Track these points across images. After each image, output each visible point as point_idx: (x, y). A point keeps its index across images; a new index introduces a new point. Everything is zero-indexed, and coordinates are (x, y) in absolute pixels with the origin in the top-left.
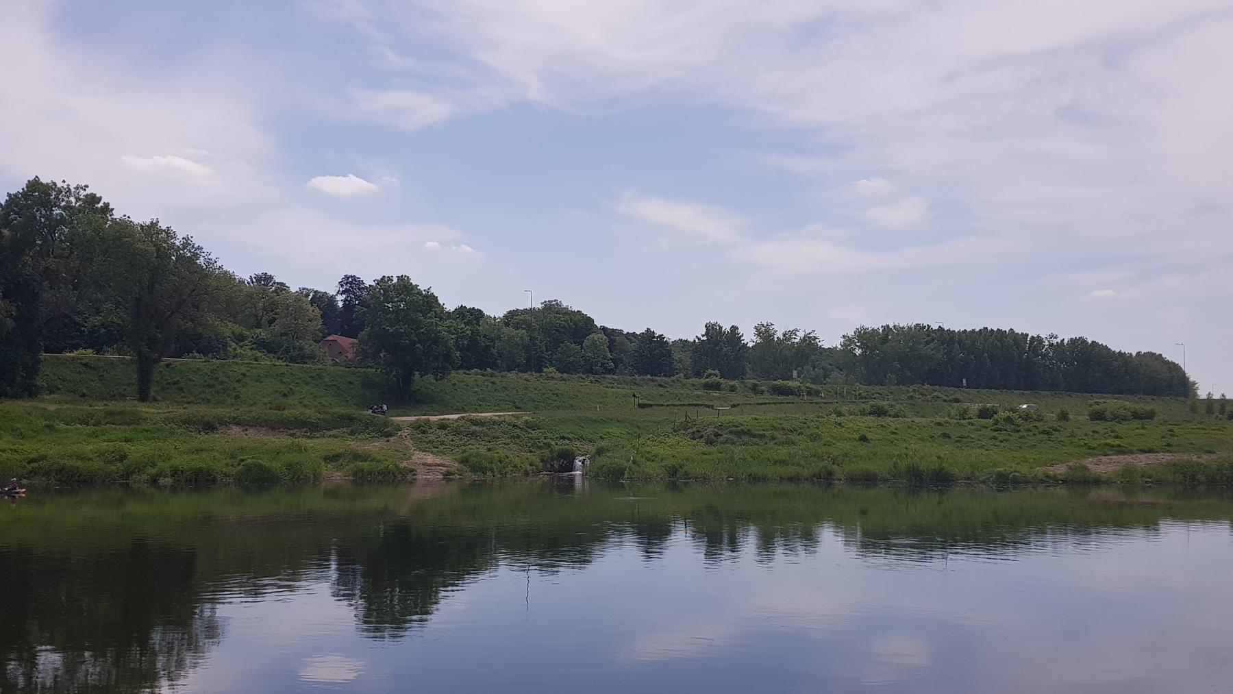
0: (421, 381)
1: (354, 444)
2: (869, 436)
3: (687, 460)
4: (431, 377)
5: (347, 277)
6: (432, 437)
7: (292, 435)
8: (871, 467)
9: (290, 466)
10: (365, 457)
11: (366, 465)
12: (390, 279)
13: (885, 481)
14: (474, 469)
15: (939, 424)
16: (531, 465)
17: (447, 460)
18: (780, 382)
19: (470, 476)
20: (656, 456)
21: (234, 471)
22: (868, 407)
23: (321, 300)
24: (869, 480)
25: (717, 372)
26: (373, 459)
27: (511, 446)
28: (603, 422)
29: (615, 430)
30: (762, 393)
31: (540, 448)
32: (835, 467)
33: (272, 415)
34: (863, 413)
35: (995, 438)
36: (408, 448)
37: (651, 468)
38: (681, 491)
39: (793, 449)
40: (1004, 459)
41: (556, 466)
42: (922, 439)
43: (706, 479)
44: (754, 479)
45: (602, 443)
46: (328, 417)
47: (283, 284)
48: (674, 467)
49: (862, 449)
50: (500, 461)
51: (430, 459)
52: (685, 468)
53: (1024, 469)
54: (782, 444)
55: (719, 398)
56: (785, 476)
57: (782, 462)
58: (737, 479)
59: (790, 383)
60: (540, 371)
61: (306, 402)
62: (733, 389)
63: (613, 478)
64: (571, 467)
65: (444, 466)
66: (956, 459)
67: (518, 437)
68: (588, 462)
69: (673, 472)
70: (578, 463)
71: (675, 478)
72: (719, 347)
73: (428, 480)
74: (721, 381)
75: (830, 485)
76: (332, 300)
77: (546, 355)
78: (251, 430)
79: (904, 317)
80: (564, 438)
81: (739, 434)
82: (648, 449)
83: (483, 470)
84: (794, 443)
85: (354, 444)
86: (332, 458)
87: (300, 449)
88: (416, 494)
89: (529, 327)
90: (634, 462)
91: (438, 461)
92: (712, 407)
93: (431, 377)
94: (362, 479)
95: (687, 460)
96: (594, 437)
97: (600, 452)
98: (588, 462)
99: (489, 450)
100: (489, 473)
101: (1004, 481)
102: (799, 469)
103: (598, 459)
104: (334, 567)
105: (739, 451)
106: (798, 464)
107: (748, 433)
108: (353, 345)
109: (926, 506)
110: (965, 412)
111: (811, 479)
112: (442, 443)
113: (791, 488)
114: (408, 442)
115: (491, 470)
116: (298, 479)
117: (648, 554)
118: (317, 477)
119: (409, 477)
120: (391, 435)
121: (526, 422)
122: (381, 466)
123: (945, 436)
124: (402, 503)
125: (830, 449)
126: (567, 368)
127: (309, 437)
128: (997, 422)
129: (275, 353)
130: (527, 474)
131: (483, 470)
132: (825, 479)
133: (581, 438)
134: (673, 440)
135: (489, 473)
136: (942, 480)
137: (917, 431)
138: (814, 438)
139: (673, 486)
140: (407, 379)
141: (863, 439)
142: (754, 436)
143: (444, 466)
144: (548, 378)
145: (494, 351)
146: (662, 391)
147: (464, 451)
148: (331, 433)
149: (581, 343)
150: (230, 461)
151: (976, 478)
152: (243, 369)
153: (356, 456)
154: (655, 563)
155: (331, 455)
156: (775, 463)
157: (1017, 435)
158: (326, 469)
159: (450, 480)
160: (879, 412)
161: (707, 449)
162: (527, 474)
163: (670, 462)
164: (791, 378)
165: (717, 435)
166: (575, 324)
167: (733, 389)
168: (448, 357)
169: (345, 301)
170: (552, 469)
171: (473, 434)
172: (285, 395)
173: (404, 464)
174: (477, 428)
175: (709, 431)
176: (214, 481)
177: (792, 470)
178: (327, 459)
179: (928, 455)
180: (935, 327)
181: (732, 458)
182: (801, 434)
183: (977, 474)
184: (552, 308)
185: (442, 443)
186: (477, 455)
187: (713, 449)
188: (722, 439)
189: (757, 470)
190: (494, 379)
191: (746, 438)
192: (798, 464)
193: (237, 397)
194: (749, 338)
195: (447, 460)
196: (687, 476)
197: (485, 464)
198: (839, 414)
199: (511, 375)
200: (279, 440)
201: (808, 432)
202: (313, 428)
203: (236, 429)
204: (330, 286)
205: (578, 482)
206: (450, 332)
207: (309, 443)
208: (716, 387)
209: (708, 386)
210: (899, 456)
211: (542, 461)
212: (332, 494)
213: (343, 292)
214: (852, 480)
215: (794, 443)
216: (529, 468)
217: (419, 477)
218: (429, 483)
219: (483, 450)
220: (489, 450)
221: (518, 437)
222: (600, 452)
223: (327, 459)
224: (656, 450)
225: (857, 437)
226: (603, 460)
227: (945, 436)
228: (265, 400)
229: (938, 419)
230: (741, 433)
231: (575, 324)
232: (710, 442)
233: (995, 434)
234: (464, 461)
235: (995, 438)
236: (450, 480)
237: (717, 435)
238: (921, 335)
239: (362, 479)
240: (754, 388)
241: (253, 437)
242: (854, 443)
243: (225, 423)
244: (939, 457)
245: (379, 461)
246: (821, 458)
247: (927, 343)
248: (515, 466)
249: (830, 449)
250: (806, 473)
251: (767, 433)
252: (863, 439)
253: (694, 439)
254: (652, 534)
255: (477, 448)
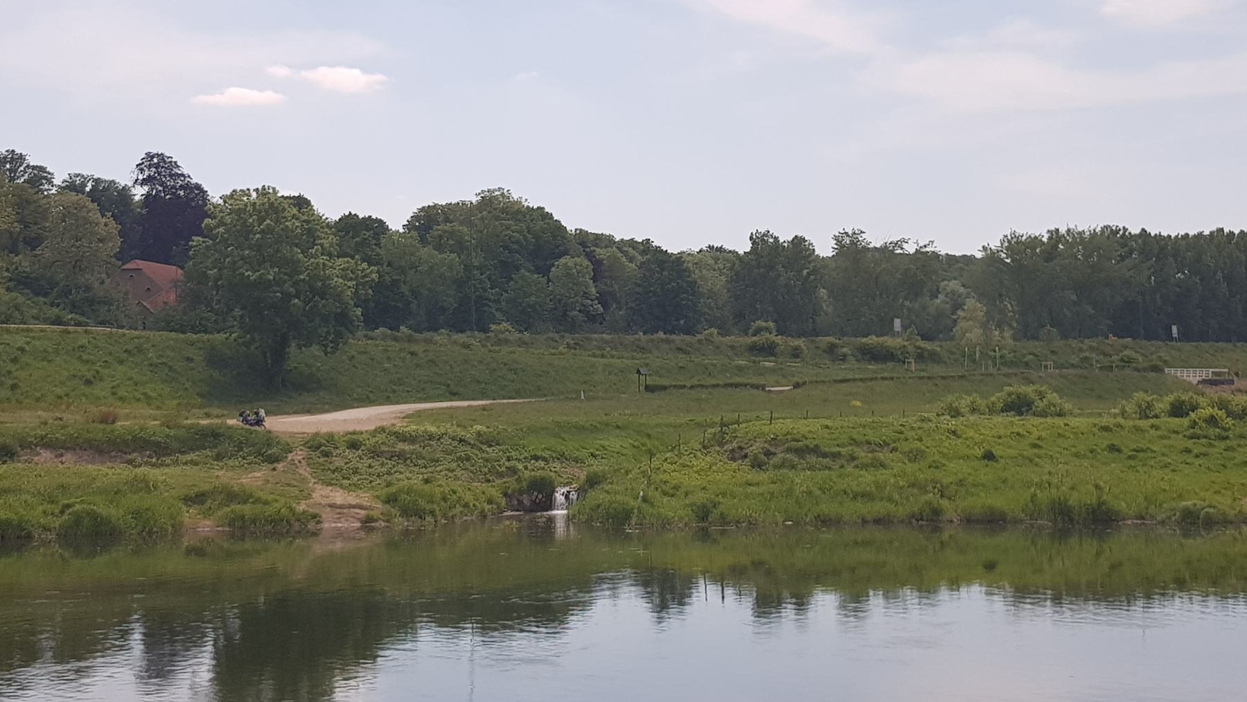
0: (302, 357)
1: (224, 475)
2: (997, 451)
3: (724, 494)
4: (315, 349)
5: (150, 156)
6: (339, 462)
7: (130, 462)
8: (998, 501)
9: (137, 514)
10: (244, 497)
11: (247, 509)
12: (246, 193)
13: (1016, 521)
14: (406, 512)
15: (1106, 429)
16: (490, 502)
17: (364, 498)
18: (872, 340)
19: (400, 523)
20: (676, 488)
21: (57, 522)
22: (998, 398)
23: (106, 196)
24: (993, 521)
25: (771, 324)
26: (258, 500)
27: (459, 473)
28: (594, 429)
29: (614, 442)
30: (844, 358)
31: (501, 475)
32: (945, 503)
33: (99, 432)
34: (992, 411)
35: (1188, 451)
36: (304, 480)
37: (671, 508)
38: (715, 541)
39: (882, 475)
40: (1196, 486)
41: (527, 502)
42: (1077, 455)
43: (752, 525)
44: (824, 522)
45: (597, 466)
46: (182, 432)
47: (42, 169)
48: (704, 506)
49: (986, 474)
50: (445, 499)
51: (339, 497)
52: (722, 508)
53: (1223, 503)
54: (865, 467)
55: (773, 371)
56: (869, 517)
57: (866, 496)
58: (797, 524)
59: (889, 341)
60: (485, 330)
61: (121, 392)
62: (796, 354)
63: (615, 523)
64: (549, 504)
65: (361, 507)
66: (1124, 486)
67: (468, 459)
68: (574, 496)
69: (703, 513)
70: (559, 497)
71: (707, 522)
72: (774, 271)
73: (339, 529)
74: (779, 339)
75: (937, 529)
76: (124, 193)
77: (492, 293)
78: (68, 457)
79: (1086, 216)
80: (536, 458)
81: (800, 452)
82: (665, 477)
83: (420, 514)
84: (883, 465)
85: (224, 475)
86: (197, 499)
87: (145, 486)
88: (318, 548)
89: (460, 247)
90: (645, 500)
91: (351, 499)
92: (763, 387)
93: (315, 349)
94: (240, 528)
95: (724, 494)
96: (584, 454)
97: (593, 481)
98: (574, 496)
99: (427, 481)
100: (429, 519)
101: (1192, 522)
102: (891, 507)
103: (591, 494)
104: (137, 636)
105: (802, 480)
106: (890, 499)
107: (816, 450)
108: (175, 283)
109: (1081, 554)
110: (1149, 406)
111: (915, 519)
112: (356, 471)
113: (879, 534)
114: (304, 471)
115: (432, 513)
116: (150, 533)
117: (661, 608)
118: (177, 529)
119: (311, 526)
120: (277, 460)
121: (479, 434)
122: (269, 511)
123: (1113, 448)
124: (294, 563)
125: (939, 475)
126: (525, 319)
127: (153, 465)
128: (1194, 424)
129: (46, 295)
130: (483, 516)
131: (420, 514)
132: (931, 520)
133: (562, 457)
134: (702, 462)
135: (429, 519)
136: (1101, 520)
137: (1070, 442)
138: (915, 456)
139: (704, 535)
140: (279, 354)
141: (989, 456)
142: (825, 455)
143: (361, 507)
144: (499, 342)
145: (405, 289)
146: (682, 359)
147: (389, 485)
148: (188, 457)
149: (544, 271)
150: (49, 507)
151: (1152, 517)
152: (20, 340)
153: (231, 496)
154: (674, 622)
155: (192, 493)
156: (855, 497)
157: (1223, 445)
158: (189, 515)
159: (372, 529)
160: (1019, 406)
161: (754, 476)
162: (483, 516)
163: (700, 497)
164: (887, 329)
165: (768, 454)
166: (537, 237)
167: (796, 354)
168: (343, 319)
169: (148, 196)
170: (520, 506)
171: (401, 456)
172: (88, 382)
173: (302, 507)
174: (406, 447)
175: (756, 448)
176: (29, 537)
177: (879, 508)
178: (189, 500)
179: (1083, 482)
180: (1135, 230)
181: (790, 492)
182: (894, 450)
183: (1152, 509)
184: (495, 207)
185: (356, 471)
186: (409, 491)
187: (763, 476)
188: (774, 460)
189: (828, 508)
190: (415, 348)
191: (812, 459)
192: (890, 499)
193: (14, 387)
194: (824, 248)
195: (364, 498)
196: (723, 519)
197: (422, 503)
198: (956, 413)
199: (441, 337)
200: (112, 472)
201: (905, 446)
202: (159, 450)
203: (46, 455)
204: (122, 171)
205: (560, 526)
206: (344, 277)
207: (154, 474)
208: (768, 350)
209: (755, 349)
210: (1040, 485)
211: (505, 495)
212: (197, 552)
213: (144, 182)
214: (969, 521)
215: (883, 465)
216: (487, 507)
217: (326, 525)
218: (339, 534)
219: (416, 481)
220: (427, 481)
221: (468, 459)
222: (593, 481)
223: (189, 500)
224: (676, 477)
225: (979, 452)
226: (598, 496)
227: (1113, 448)
228: (59, 391)
229: (1106, 421)
230: (805, 451)
231: (537, 237)
232: (758, 465)
233: (1189, 444)
234: (391, 500)
235: (1188, 451)
236: (372, 529)
237: (768, 454)
238: (1115, 244)
239: (240, 528)
240: (831, 349)
241: (73, 468)
242: (976, 463)
243: (29, 444)
244: (1097, 487)
245: (266, 503)
246: (923, 489)
247: (1123, 258)
248: (466, 505)
249: (939, 475)
250: (901, 512)
251: (843, 451)
252: (989, 456)
253: (733, 459)
254: (667, 591)
255: (408, 478)
